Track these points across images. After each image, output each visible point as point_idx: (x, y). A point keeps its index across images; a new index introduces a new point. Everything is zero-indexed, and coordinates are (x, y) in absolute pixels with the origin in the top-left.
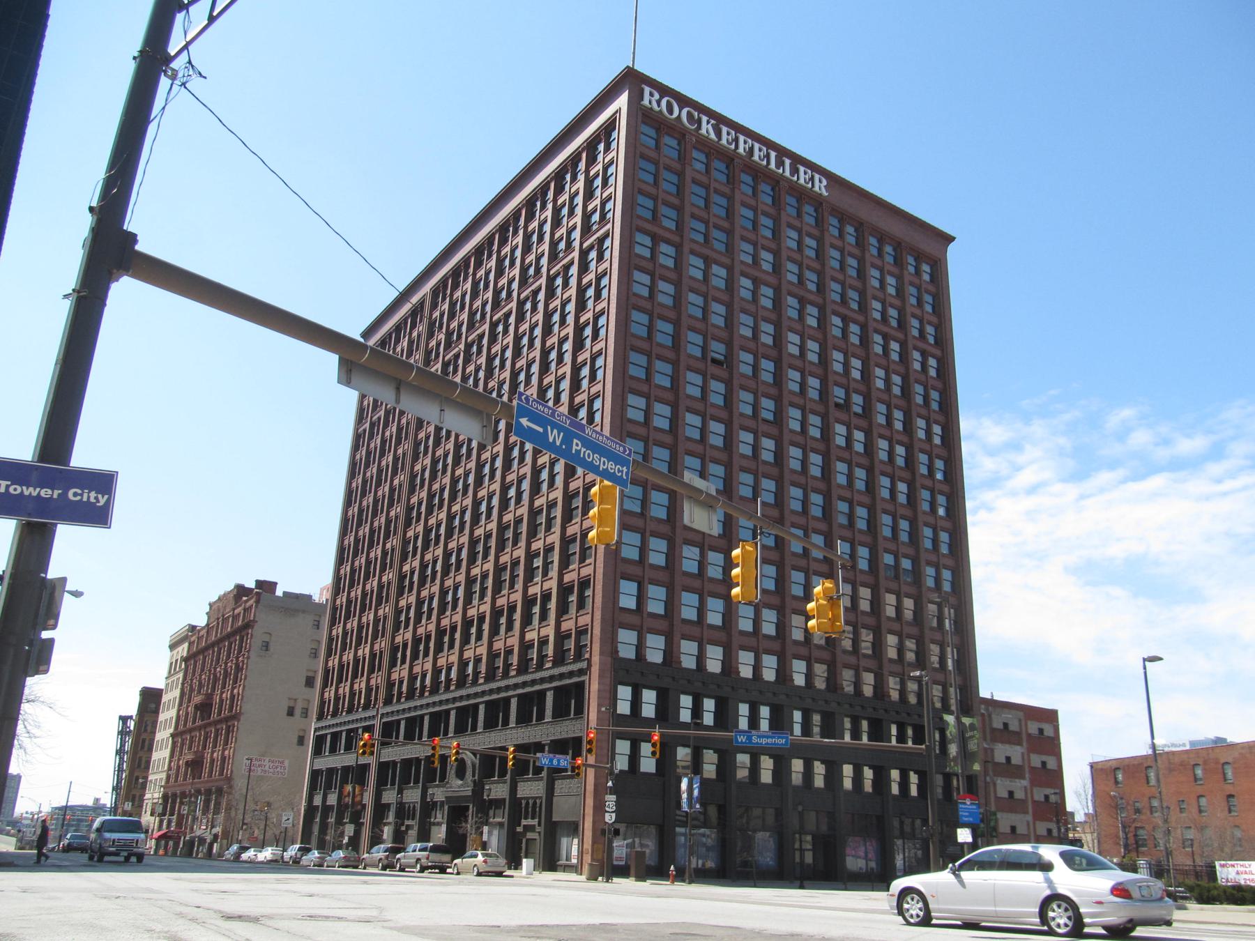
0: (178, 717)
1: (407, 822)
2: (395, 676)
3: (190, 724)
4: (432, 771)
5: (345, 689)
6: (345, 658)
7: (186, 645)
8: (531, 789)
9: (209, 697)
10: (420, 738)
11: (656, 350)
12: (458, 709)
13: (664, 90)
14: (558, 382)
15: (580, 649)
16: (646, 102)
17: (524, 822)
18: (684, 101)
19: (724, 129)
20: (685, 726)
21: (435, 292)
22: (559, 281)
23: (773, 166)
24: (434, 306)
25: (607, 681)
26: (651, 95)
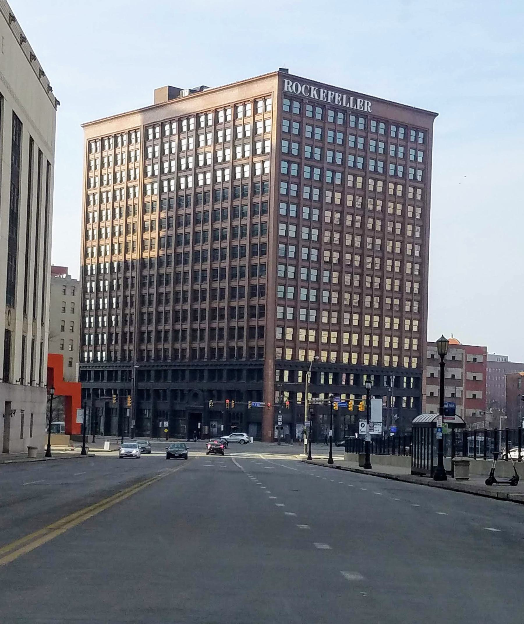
16: (286, 89)
23: (344, 104)
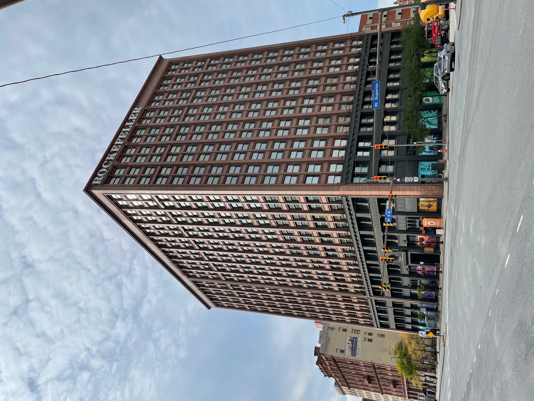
0: (374, 391)
1: (419, 284)
2: (353, 290)
3: (377, 386)
4: (393, 270)
5: (359, 314)
6: (345, 314)
7: (343, 388)
8: (402, 223)
9: (364, 377)
10: (380, 278)
11: (207, 174)
12: (366, 260)
13: (95, 175)
14: (241, 245)
15: (338, 202)
16: (99, 182)
17: (418, 226)
18: (100, 167)
19: (112, 150)
20: (371, 154)
21: (189, 276)
22: (191, 233)
23: (128, 130)
24: (194, 277)
25: (351, 187)
26: (96, 180)
